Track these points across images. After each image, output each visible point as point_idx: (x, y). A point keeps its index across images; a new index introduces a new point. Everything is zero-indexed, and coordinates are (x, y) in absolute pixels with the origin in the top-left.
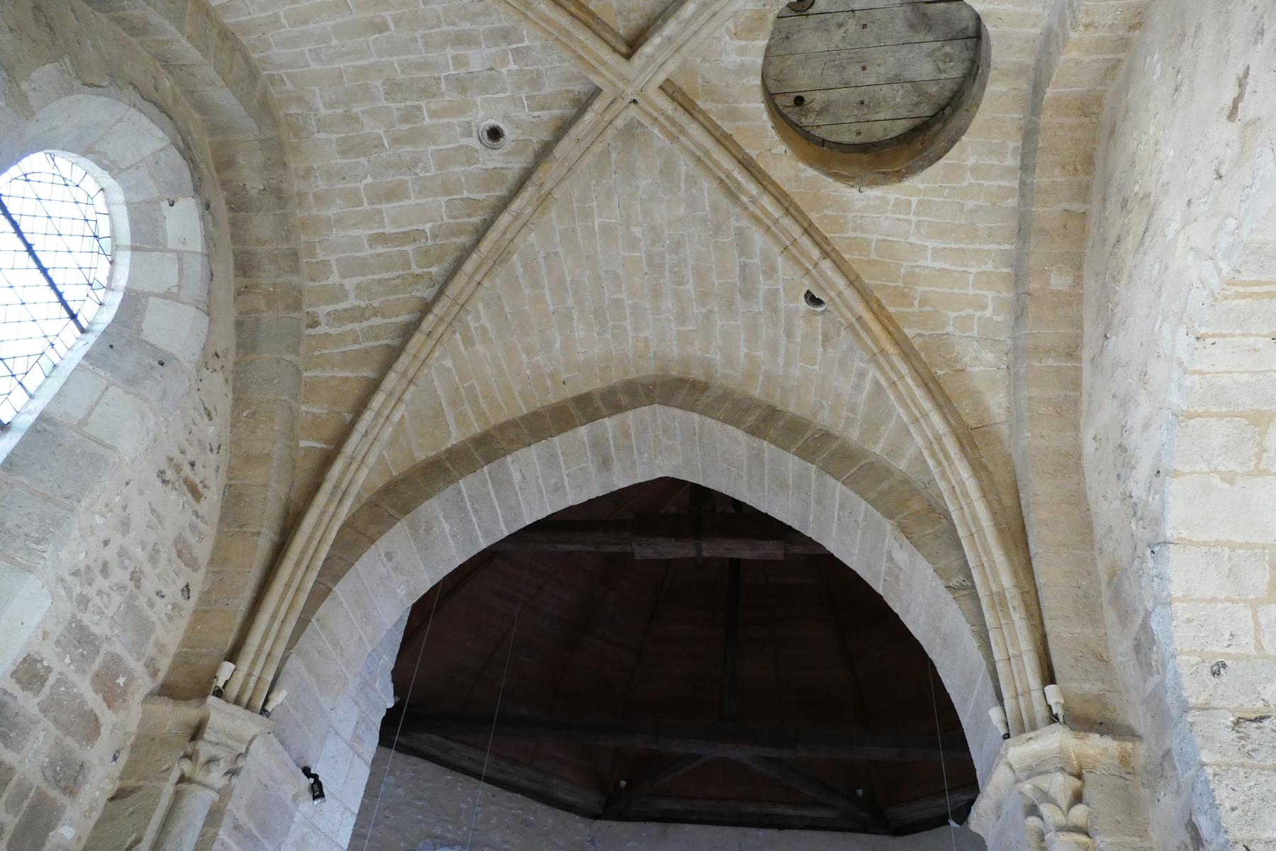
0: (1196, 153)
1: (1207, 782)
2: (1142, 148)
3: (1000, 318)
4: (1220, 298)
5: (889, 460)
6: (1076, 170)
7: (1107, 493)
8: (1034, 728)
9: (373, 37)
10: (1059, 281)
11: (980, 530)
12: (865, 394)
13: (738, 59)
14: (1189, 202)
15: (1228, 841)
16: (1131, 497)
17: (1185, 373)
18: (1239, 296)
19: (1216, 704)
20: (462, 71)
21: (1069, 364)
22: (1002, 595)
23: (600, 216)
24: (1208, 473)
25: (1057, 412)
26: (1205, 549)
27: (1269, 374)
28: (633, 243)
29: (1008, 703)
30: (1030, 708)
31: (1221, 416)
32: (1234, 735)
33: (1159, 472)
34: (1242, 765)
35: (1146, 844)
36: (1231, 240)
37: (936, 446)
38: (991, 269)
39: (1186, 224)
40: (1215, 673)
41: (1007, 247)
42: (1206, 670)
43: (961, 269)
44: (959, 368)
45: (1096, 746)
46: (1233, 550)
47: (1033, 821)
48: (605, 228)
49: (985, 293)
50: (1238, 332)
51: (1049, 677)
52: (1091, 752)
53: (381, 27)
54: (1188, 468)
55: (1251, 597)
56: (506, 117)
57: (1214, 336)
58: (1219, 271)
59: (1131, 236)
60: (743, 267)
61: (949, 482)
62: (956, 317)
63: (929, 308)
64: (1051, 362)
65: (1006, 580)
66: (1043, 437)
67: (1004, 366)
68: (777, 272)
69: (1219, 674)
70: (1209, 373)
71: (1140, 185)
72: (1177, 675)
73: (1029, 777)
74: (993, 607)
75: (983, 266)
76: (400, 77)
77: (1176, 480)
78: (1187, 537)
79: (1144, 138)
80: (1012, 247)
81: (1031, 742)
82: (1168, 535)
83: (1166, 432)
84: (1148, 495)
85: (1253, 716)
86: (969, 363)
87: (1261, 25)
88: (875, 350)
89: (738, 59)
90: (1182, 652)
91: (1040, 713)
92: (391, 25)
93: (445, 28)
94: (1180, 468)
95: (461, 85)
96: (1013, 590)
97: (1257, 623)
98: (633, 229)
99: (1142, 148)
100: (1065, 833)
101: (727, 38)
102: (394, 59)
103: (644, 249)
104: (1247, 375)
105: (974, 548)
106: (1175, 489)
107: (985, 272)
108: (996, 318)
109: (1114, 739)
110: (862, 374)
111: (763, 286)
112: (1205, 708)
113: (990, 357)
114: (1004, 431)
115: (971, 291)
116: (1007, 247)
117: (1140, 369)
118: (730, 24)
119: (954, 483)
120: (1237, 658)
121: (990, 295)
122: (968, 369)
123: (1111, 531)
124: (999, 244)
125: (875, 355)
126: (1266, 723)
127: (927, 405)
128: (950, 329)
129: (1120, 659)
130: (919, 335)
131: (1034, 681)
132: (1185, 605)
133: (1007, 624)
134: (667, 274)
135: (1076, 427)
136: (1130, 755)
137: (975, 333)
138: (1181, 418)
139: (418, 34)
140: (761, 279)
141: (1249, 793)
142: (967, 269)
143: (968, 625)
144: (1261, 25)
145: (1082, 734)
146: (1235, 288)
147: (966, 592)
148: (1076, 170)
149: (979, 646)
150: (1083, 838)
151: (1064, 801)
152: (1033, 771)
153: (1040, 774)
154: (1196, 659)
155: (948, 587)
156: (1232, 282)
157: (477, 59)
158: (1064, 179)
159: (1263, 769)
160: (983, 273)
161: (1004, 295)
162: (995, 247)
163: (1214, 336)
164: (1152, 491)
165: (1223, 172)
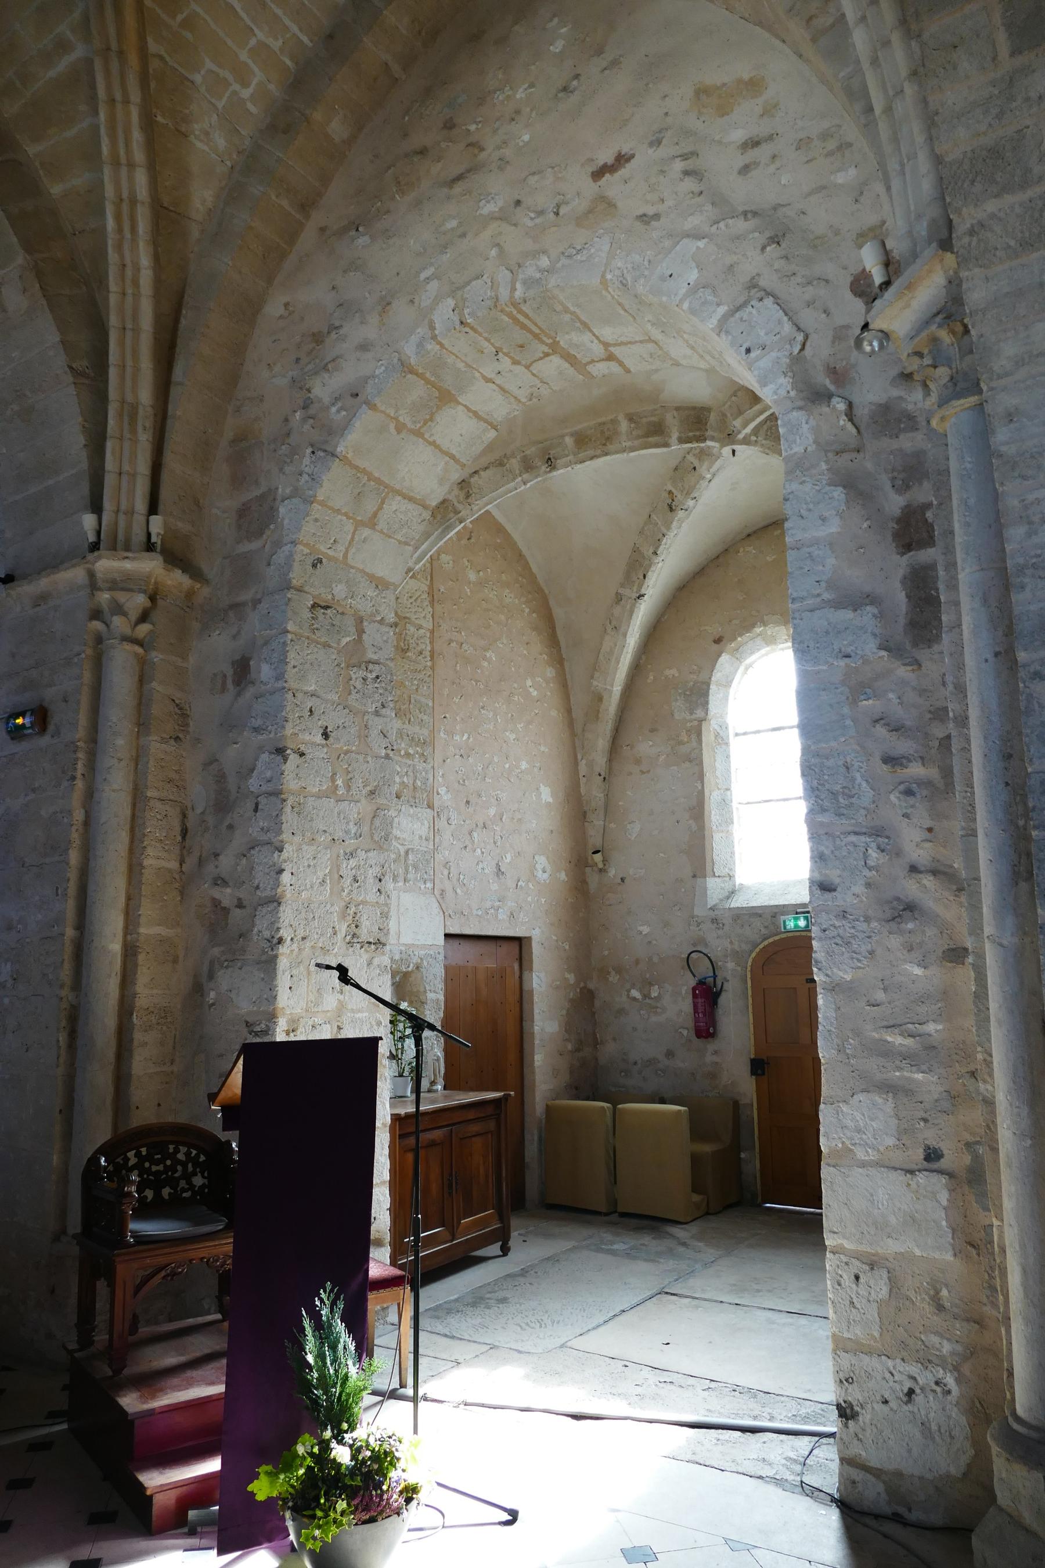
0: (550, 170)
1: (285, 644)
2: (501, 98)
3: (253, 109)
4: (499, 308)
5: (41, 172)
6: (420, 32)
7: (274, 364)
8: (127, 548)
10: (337, 129)
11: (136, 330)
12: (52, 73)
14: (518, 203)
15: (284, 688)
16: (309, 391)
17: (432, 338)
18: (510, 315)
19: (306, 589)
21: (298, 216)
22: (134, 409)
24: (392, 418)
25: (264, 255)
26: (354, 471)
27: (474, 371)
29: (106, 517)
30: (129, 527)
31: (428, 382)
32: (310, 615)
33: (357, 395)
34: (308, 638)
35: (185, 665)
36: (538, 275)
37: (125, 208)
38: (277, 49)
39: (502, 217)
40: (314, 566)
41: (305, 39)
42: (309, 561)
43: (249, 22)
44: (183, 130)
45: (177, 579)
46: (369, 480)
47: (97, 625)
49: (256, 69)
50: (486, 335)
51: (153, 508)
52: (169, 582)
54: (383, 408)
55: (359, 518)
57: (472, 328)
58: (513, 289)
59: (440, 165)
61: (122, 257)
62: (212, 71)
63: (188, 35)
64: (285, 203)
65: (145, 395)
66: (240, 272)
67: (229, 163)
69: (316, 567)
70: (446, 349)
71: (477, 129)
72: (290, 556)
73: (110, 589)
74: (120, 415)
75: (271, 39)
77: (370, 412)
78: (350, 459)
79: (508, 92)
80: (310, 45)
81: (126, 560)
82: (339, 449)
83: (383, 368)
84: (333, 404)
85: (323, 604)
86: (197, 133)
87: (662, 135)
88: (114, 45)
90: (301, 543)
91: (138, 536)
94: (379, 405)
96: (150, 410)
97: (353, 539)
99: (501, 98)
100: (130, 644)
104: (463, 364)
105: (122, 343)
106: (365, 420)
107: (269, 47)
108: (250, 106)
109: (191, 577)
110: (63, 46)
112: (300, 590)
113: (221, 142)
114: (195, 233)
115: (244, 56)
116: (305, 39)
117: (384, 293)
119: (128, 261)
120: (330, 559)
121: (258, 76)
122: (192, 138)
123: (262, 401)
124: (301, 30)
125: (109, 49)
126: (329, 611)
127: (139, 156)
128: (198, 78)
129: (215, 511)
130: (161, 58)
131: (141, 506)
132: (320, 507)
133: (130, 439)
135: (270, 280)
136: (194, 592)
137: (220, 105)
138: (406, 369)
141: (305, 658)
142: (254, 28)
143: (80, 419)
144: (662, 135)
145: (170, 566)
146: (513, 310)
147: (86, 382)
148: (420, 32)
149: (85, 446)
150: (139, 650)
151: (134, 616)
152: (114, 585)
153: (123, 589)
154: (306, 551)
155: (71, 368)
156: (515, 305)
158: (404, 32)
159: (318, 643)
160: (267, 46)
161: (271, 87)
162: (295, 29)
163: (472, 328)
164: (340, 404)
165: (562, 212)
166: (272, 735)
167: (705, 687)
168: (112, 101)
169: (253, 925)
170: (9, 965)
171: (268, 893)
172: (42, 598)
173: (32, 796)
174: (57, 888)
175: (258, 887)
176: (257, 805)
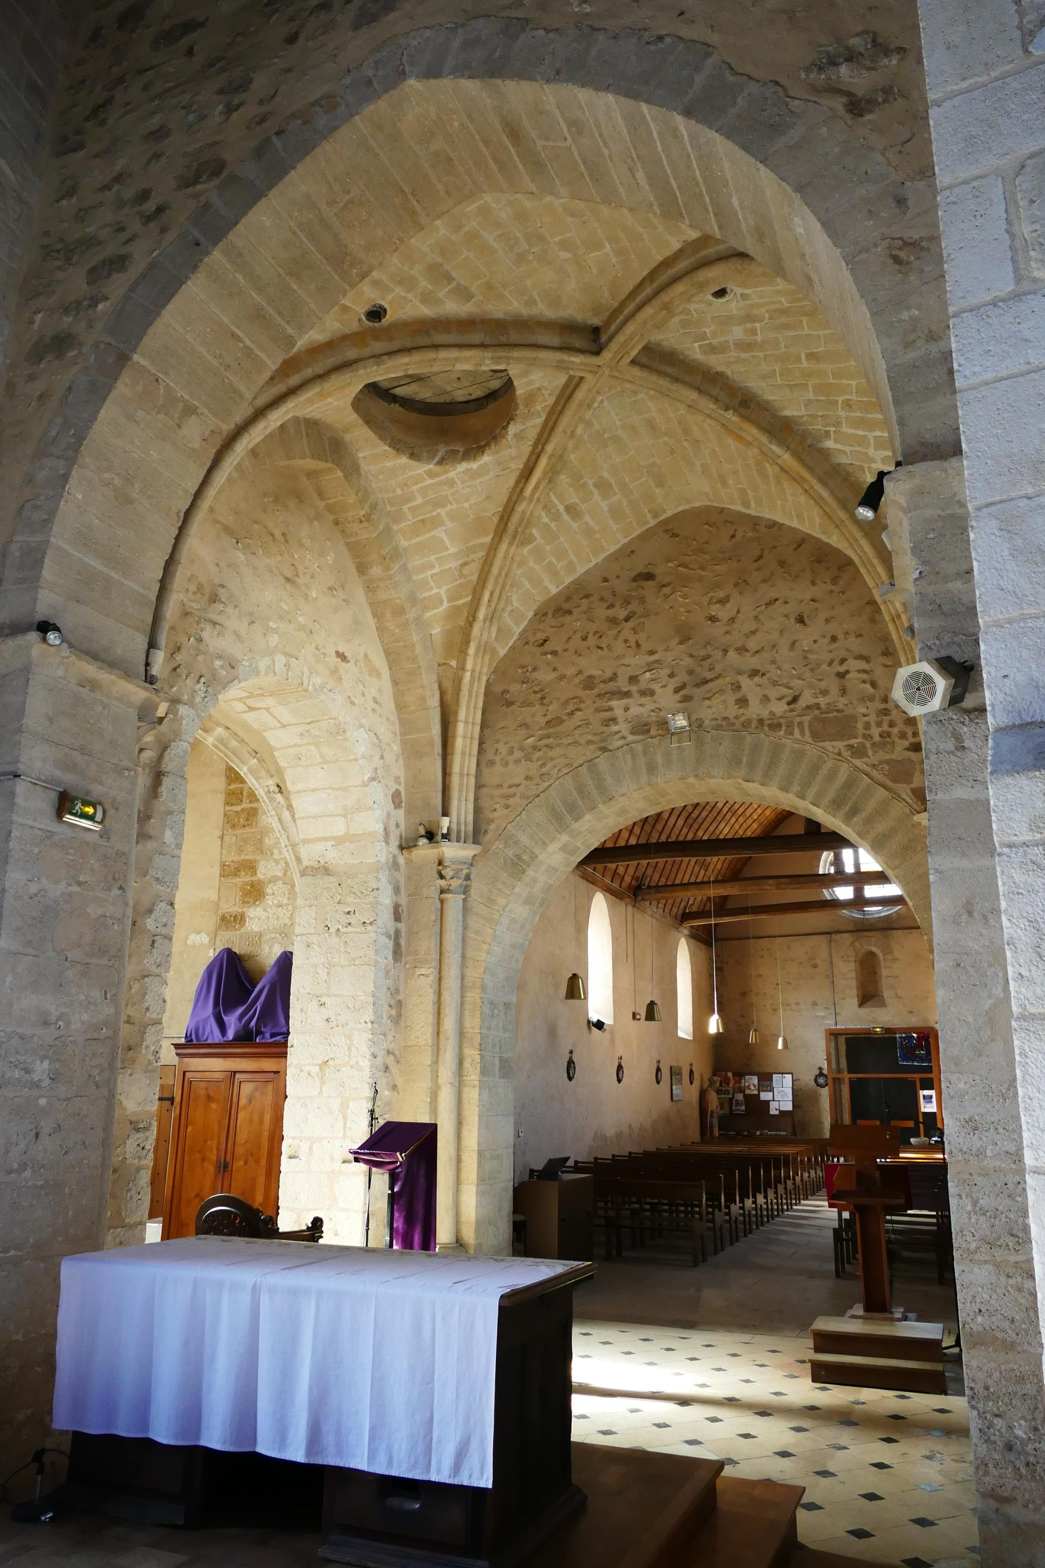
9: (820, 349)
13: (531, 377)
20: (749, 325)
23: (607, 254)
28: (564, 245)
48: (597, 246)
53: (810, 356)
56: (710, 304)
60: (450, 279)
68: (420, 301)
76: (805, 320)
89: (531, 377)
92: (803, 357)
93: (761, 354)
95: (750, 318)
98: (570, 255)
101: (545, 385)
102: (806, 331)
103: (552, 245)
111: (424, 284)
118: (546, 393)
134: (518, 235)
139: (783, 350)
140: (430, 287)
157: (737, 333)
166: (168, 890)
167: (945, 1220)
168: (473, 724)
169: (143, 1040)
170: (46, 1063)
171: (154, 1016)
172: (93, 685)
173: (75, 889)
174: (106, 992)
175: (147, 1009)
176: (153, 942)
